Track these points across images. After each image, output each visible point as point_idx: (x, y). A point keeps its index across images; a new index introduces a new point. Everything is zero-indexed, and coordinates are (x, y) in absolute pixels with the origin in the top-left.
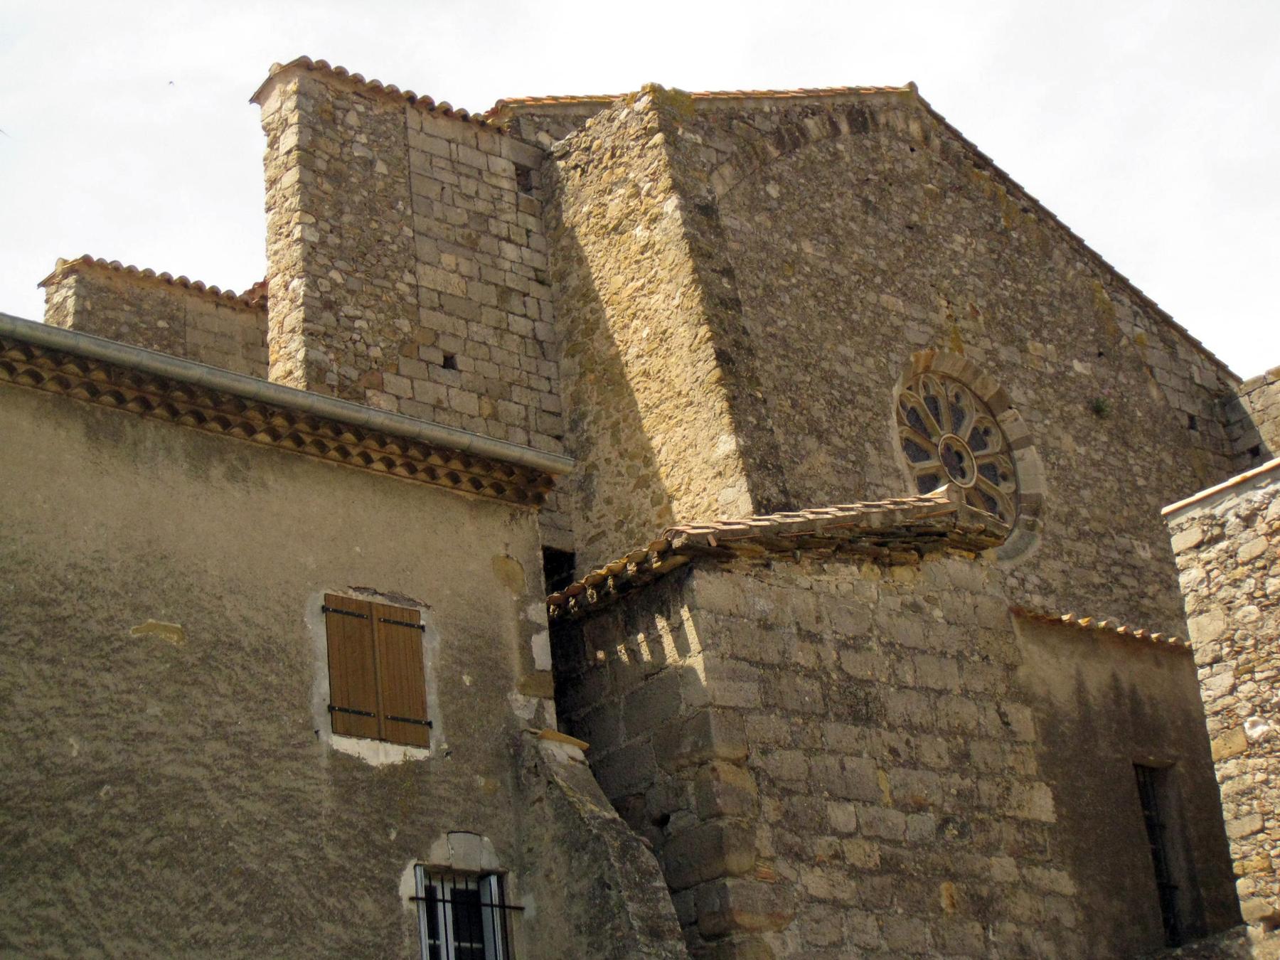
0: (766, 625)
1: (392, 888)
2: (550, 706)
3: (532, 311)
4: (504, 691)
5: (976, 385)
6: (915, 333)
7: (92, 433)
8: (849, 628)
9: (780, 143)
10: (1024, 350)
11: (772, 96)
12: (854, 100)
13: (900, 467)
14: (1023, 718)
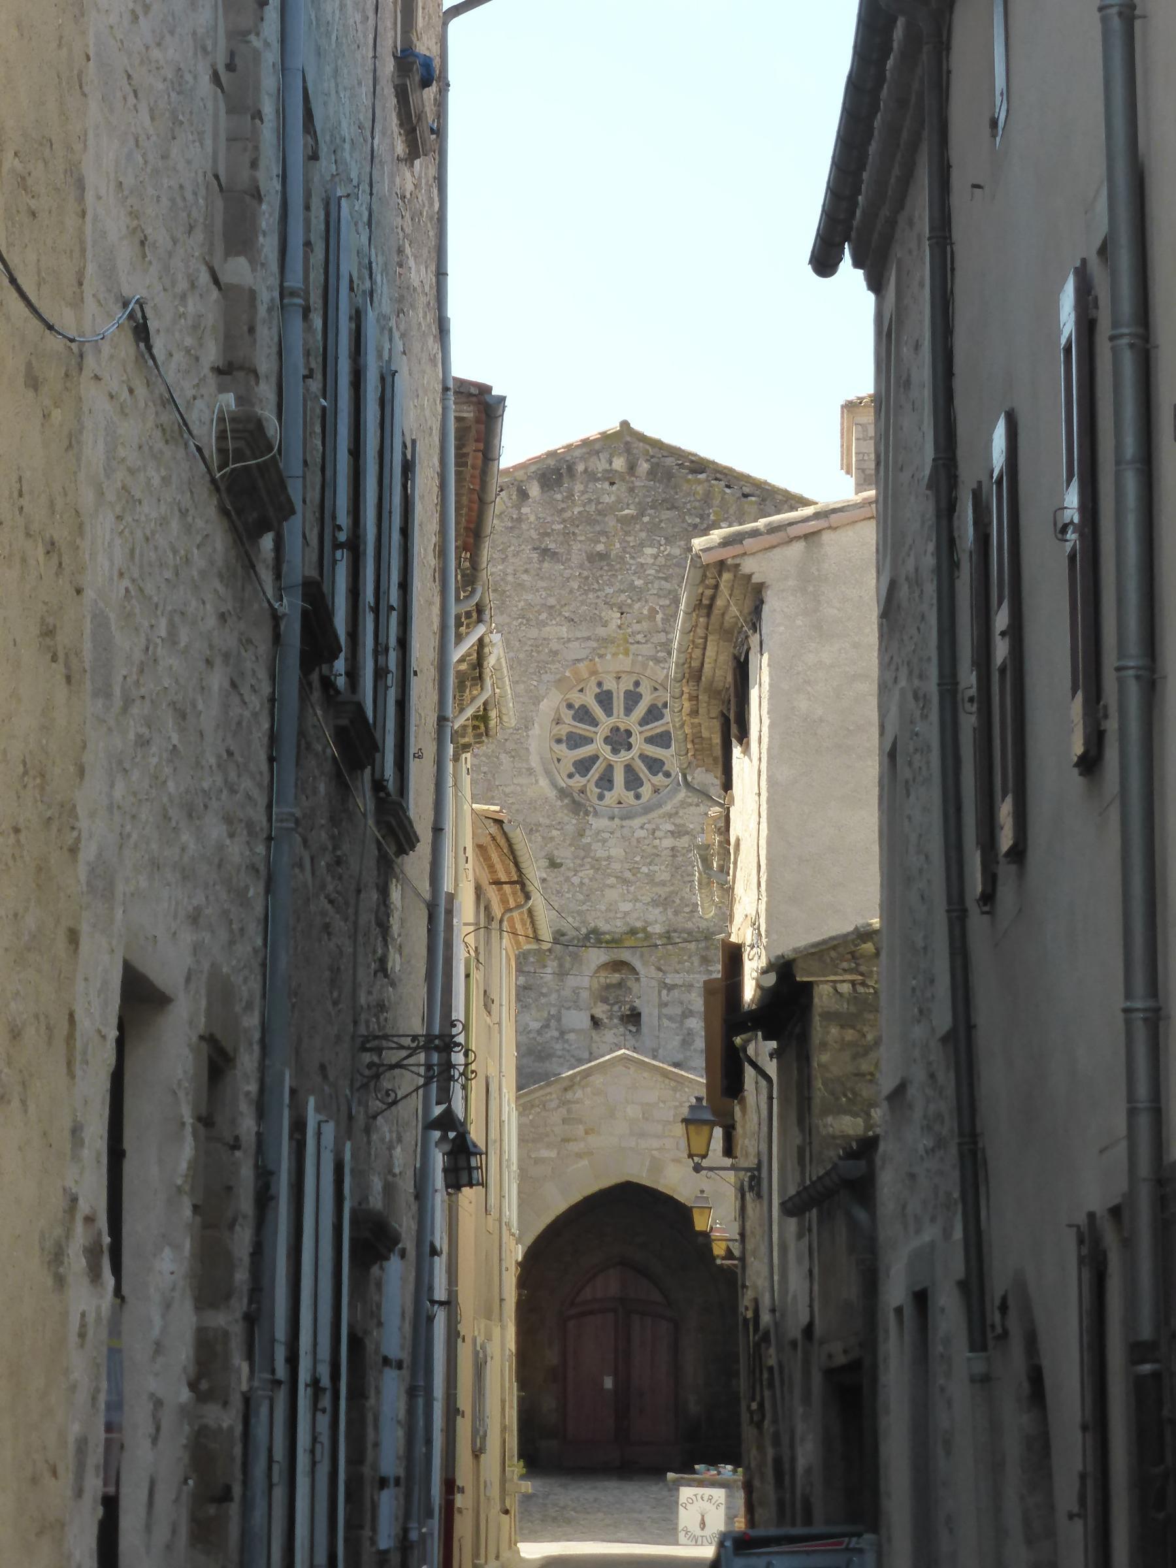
12: (552, 462)
13: (533, 765)
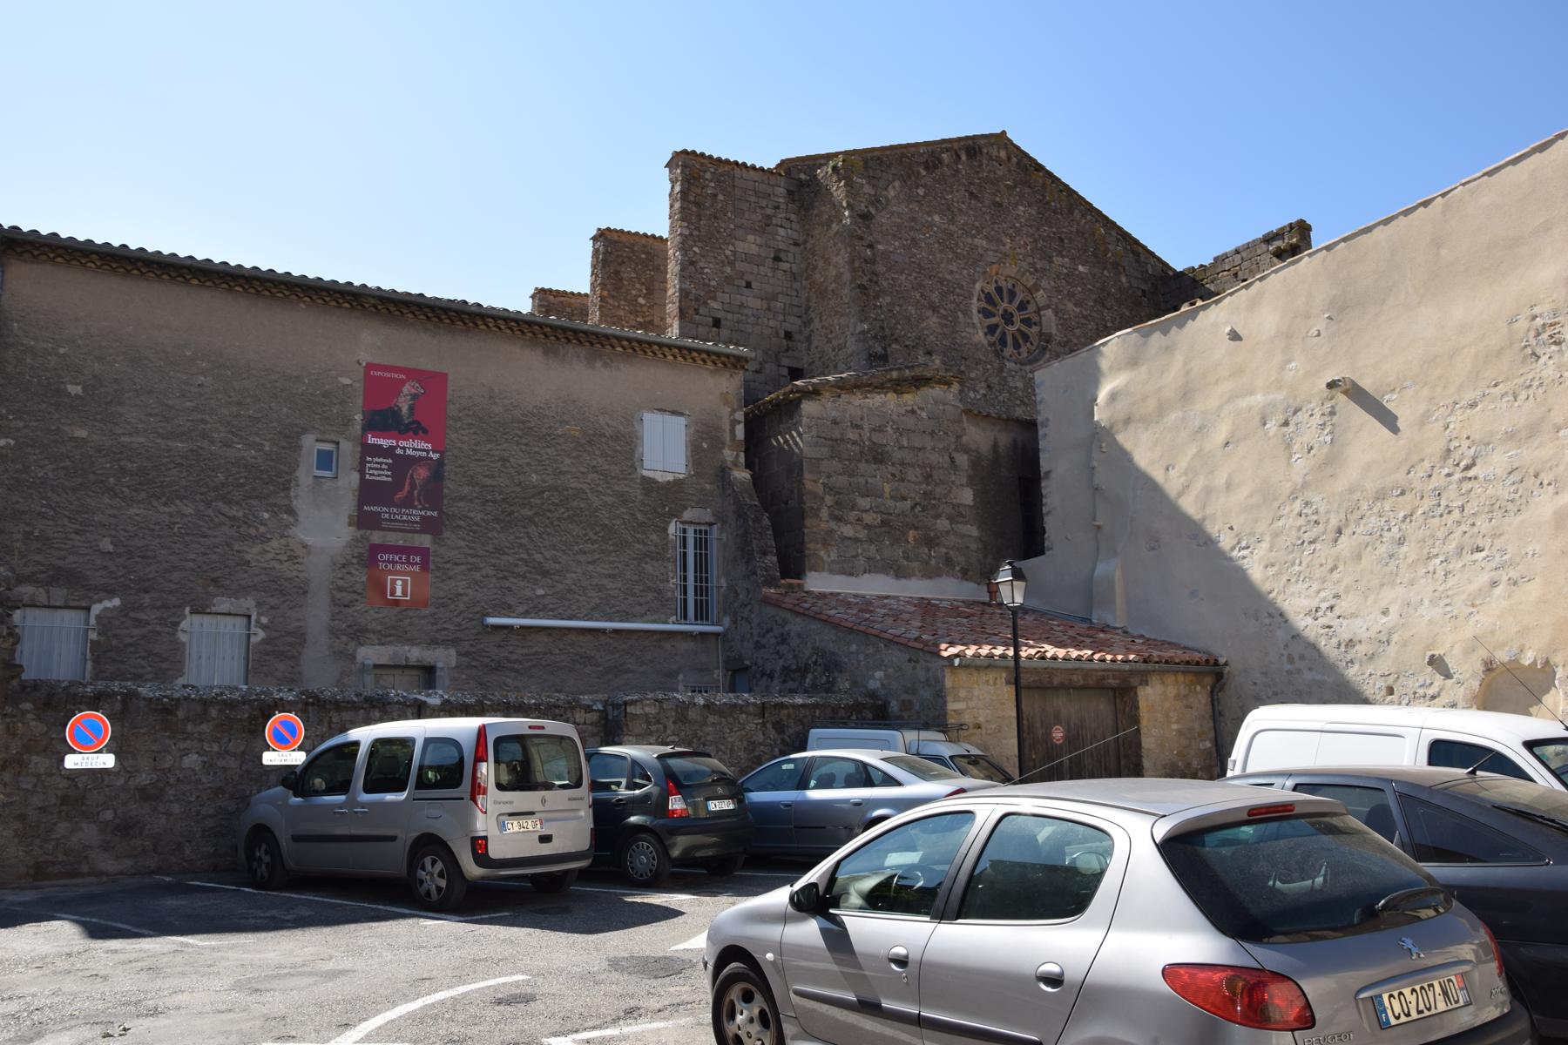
0: (835, 422)
1: (665, 530)
2: (742, 455)
3: (791, 259)
4: (720, 450)
5: (1023, 280)
6: (990, 256)
7: (546, 352)
8: (878, 422)
9: (927, 168)
10: (1051, 262)
11: (926, 144)
14: (962, 459)
